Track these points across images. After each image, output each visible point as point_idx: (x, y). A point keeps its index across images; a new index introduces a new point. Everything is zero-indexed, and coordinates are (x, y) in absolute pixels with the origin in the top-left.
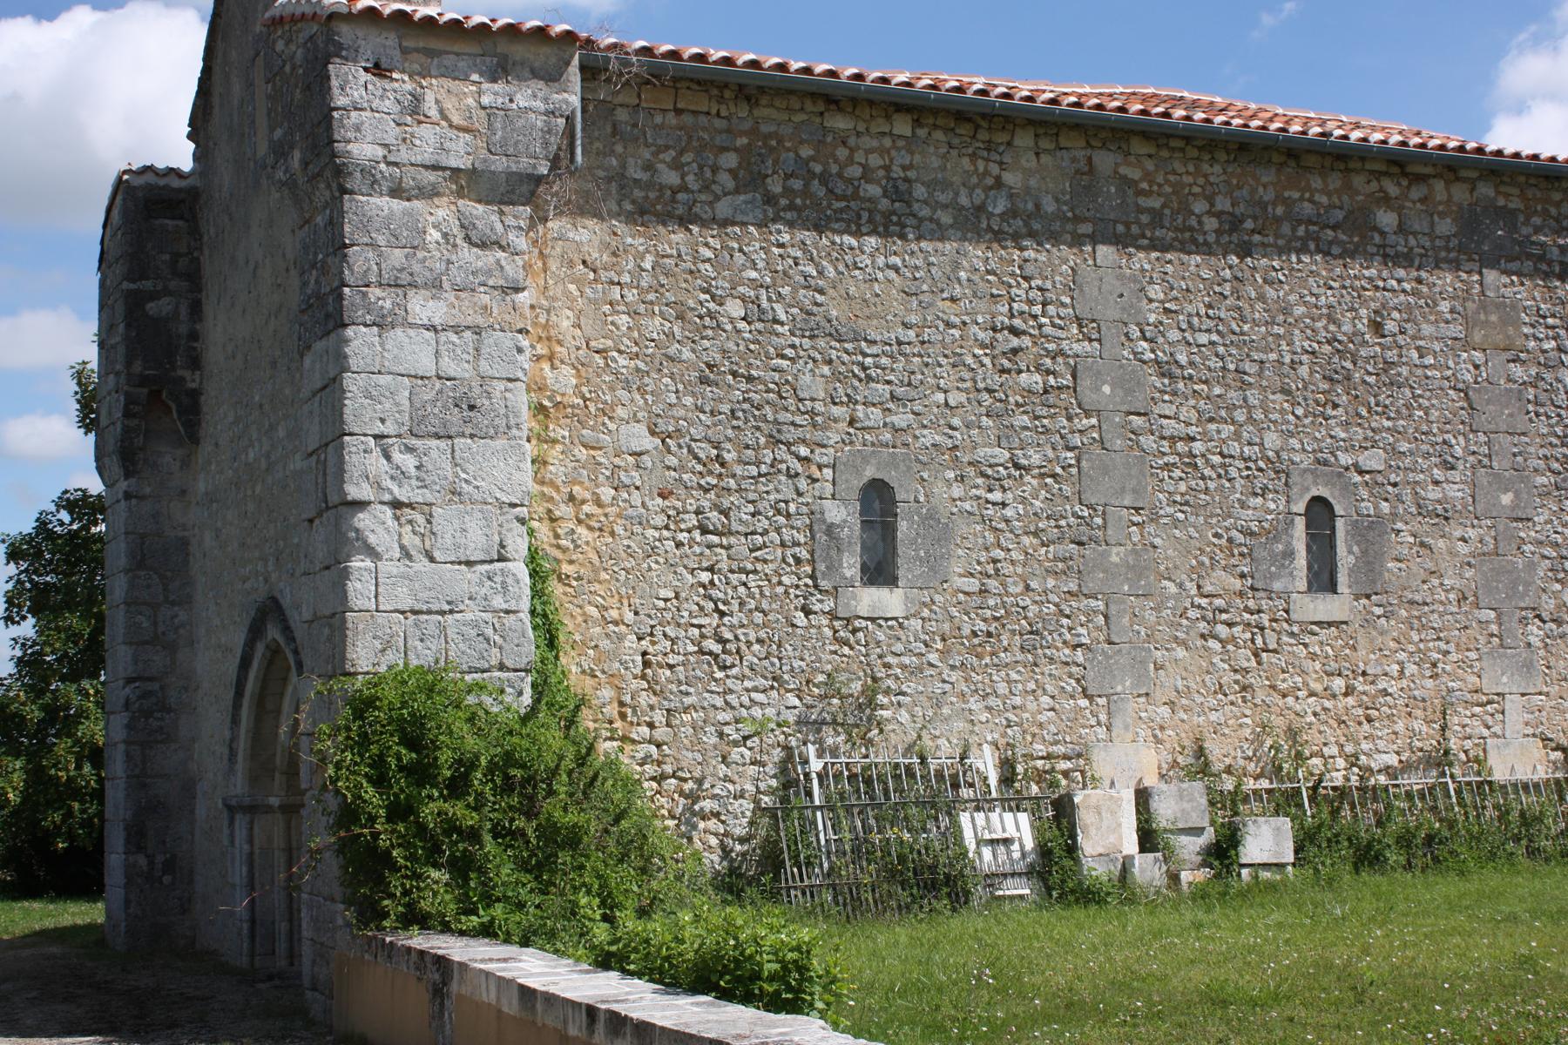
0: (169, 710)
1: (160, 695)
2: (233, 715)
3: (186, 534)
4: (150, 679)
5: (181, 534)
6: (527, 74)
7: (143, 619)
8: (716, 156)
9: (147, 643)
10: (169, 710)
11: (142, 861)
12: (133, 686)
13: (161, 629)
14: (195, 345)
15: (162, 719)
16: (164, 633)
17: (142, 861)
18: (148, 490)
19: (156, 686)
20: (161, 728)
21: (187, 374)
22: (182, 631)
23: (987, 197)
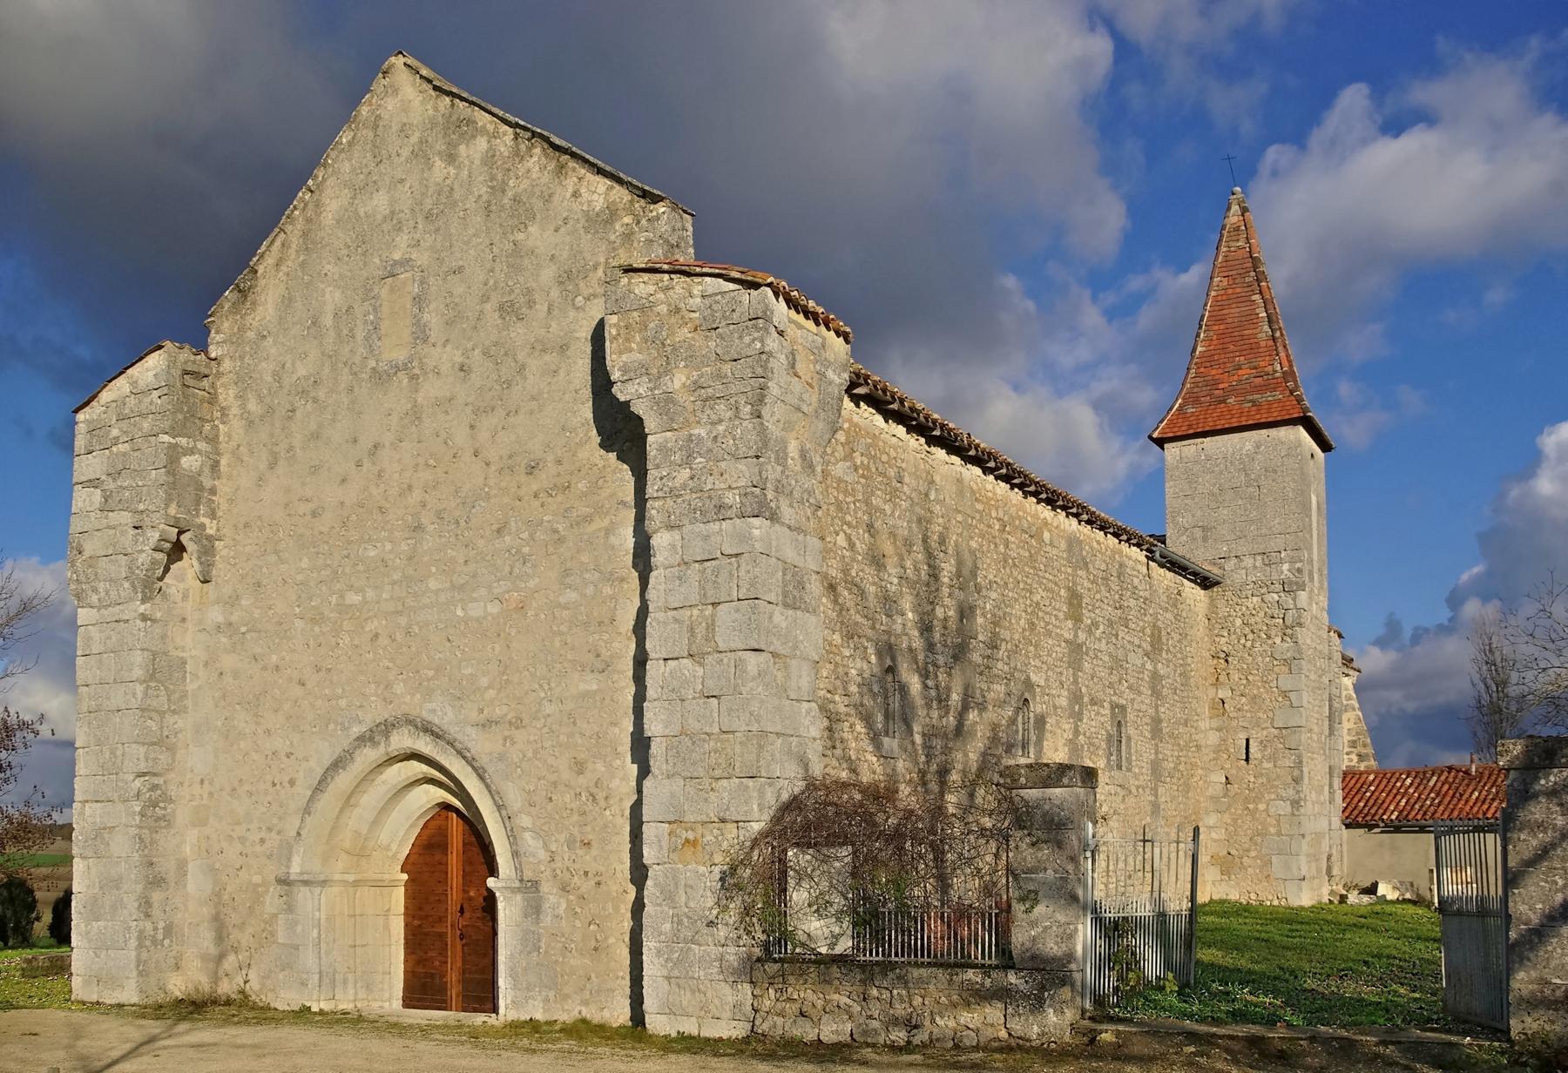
0: (171, 801)
1: (163, 788)
2: (594, 353)
3: (184, 655)
4: (155, 775)
5: (181, 655)
6: (1545, 921)
7: (153, 724)
8: (1069, 895)
9: (154, 744)
10: (171, 801)
11: (149, 926)
12: (142, 779)
13: (165, 733)
14: (214, 498)
15: (165, 809)
16: (167, 737)
17: (149, 926)
18: (159, 615)
19: (160, 781)
20: (164, 816)
21: (206, 521)
22: (180, 735)
23: (929, 488)
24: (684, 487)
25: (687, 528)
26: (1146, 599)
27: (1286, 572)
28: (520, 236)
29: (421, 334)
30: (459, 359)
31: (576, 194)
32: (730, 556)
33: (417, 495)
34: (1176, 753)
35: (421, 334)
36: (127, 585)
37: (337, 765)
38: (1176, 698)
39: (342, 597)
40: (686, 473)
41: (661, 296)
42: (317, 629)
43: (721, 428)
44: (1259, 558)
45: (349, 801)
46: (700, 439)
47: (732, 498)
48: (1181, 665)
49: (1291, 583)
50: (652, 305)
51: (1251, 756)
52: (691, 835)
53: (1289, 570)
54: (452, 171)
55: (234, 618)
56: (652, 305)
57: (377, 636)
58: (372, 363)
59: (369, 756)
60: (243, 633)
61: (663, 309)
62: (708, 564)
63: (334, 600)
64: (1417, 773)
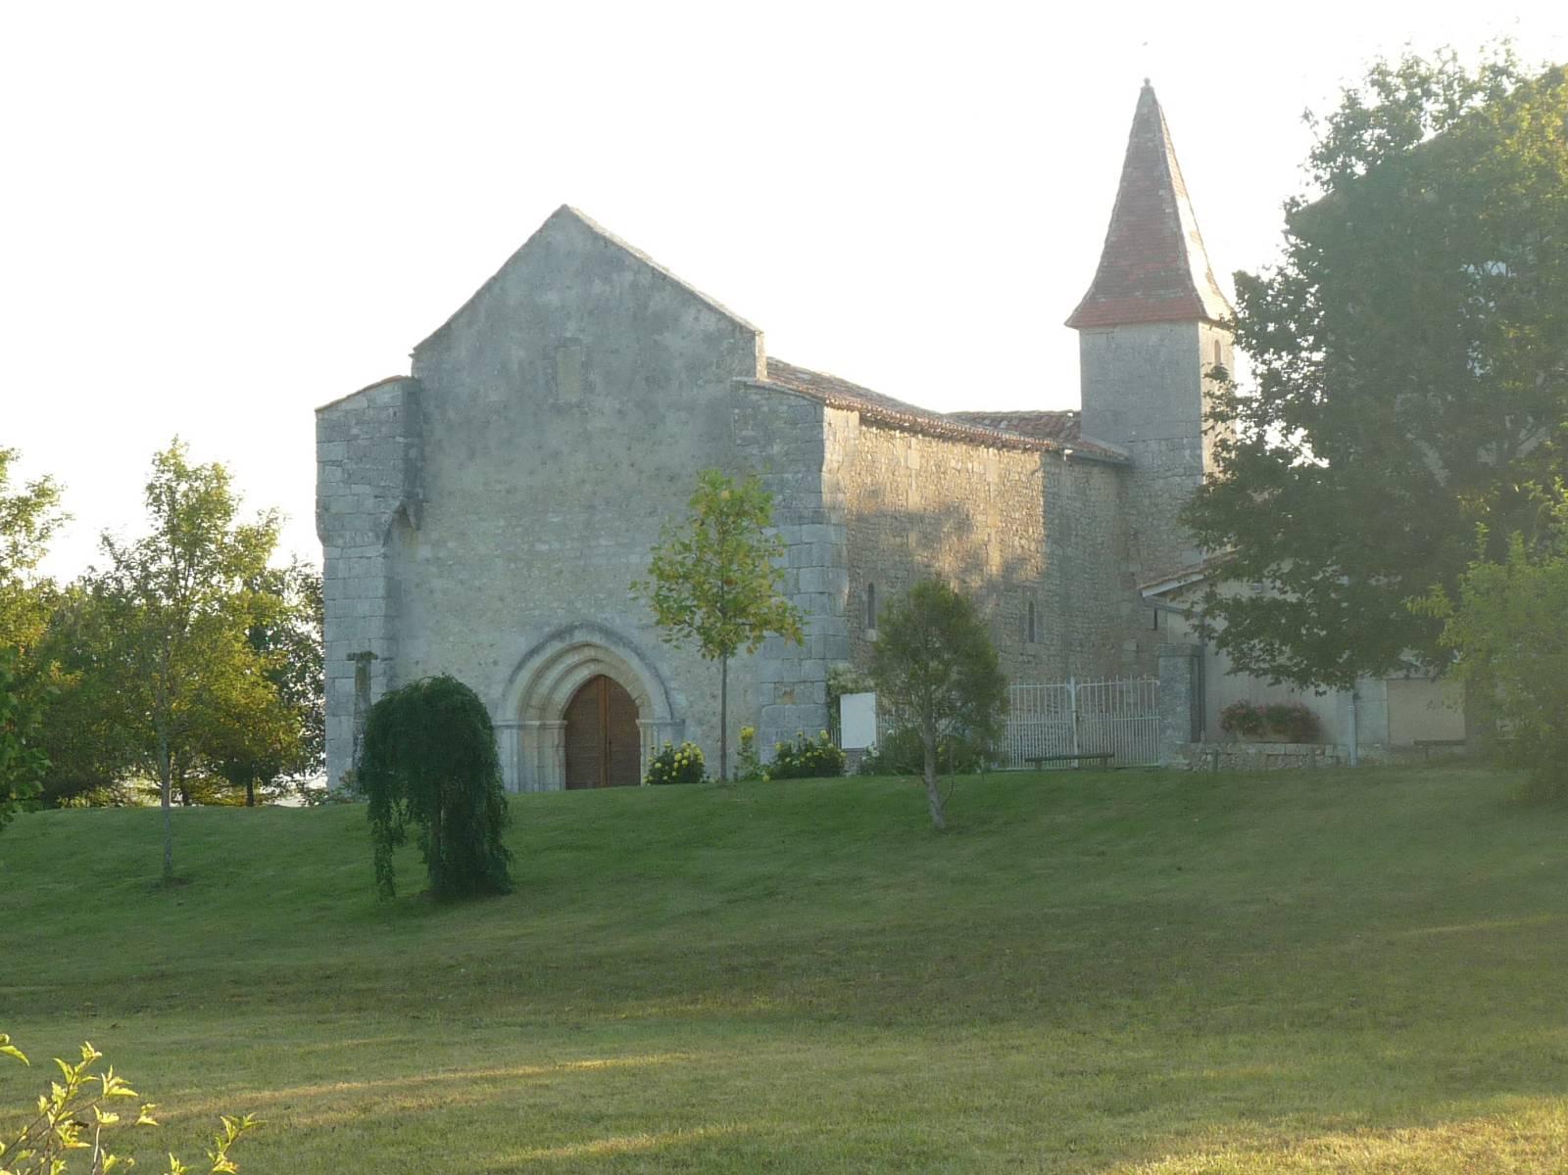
24: (779, 504)
25: (782, 527)
26: (1055, 494)
27: (1188, 458)
28: (657, 337)
29: (589, 387)
30: (618, 406)
31: (696, 319)
32: (807, 544)
33: (588, 488)
34: (1086, 625)
35: (589, 387)
36: (370, 534)
37: (533, 652)
38: (1086, 576)
39: (533, 545)
40: (781, 497)
41: (764, 402)
42: (513, 566)
43: (800, 476)
44: (1163, 442)
45: (539, 674)
46: (788, 480)
47: (806, 513)
48: (1091, 545)
49: (1191, 467)
50: (760, 406)
51: (1159, 625)
52: (788, 689)
53: (1191, 456)
54: (608, 288)
55: (441, 555)
56: (760, 406)
57: (561, 572)
58: (551, 401)
59: (557, 646)
60: (450, 566)
61: (766, 409)
62: (793, 547)
63: (526, 547)
64: (324, 731)
